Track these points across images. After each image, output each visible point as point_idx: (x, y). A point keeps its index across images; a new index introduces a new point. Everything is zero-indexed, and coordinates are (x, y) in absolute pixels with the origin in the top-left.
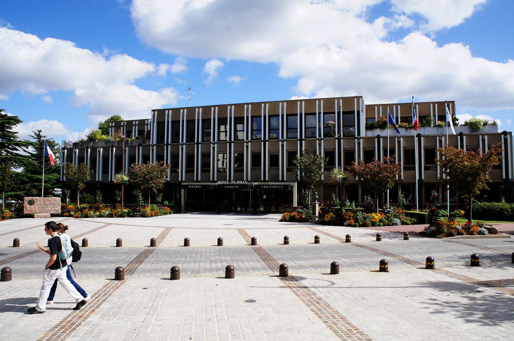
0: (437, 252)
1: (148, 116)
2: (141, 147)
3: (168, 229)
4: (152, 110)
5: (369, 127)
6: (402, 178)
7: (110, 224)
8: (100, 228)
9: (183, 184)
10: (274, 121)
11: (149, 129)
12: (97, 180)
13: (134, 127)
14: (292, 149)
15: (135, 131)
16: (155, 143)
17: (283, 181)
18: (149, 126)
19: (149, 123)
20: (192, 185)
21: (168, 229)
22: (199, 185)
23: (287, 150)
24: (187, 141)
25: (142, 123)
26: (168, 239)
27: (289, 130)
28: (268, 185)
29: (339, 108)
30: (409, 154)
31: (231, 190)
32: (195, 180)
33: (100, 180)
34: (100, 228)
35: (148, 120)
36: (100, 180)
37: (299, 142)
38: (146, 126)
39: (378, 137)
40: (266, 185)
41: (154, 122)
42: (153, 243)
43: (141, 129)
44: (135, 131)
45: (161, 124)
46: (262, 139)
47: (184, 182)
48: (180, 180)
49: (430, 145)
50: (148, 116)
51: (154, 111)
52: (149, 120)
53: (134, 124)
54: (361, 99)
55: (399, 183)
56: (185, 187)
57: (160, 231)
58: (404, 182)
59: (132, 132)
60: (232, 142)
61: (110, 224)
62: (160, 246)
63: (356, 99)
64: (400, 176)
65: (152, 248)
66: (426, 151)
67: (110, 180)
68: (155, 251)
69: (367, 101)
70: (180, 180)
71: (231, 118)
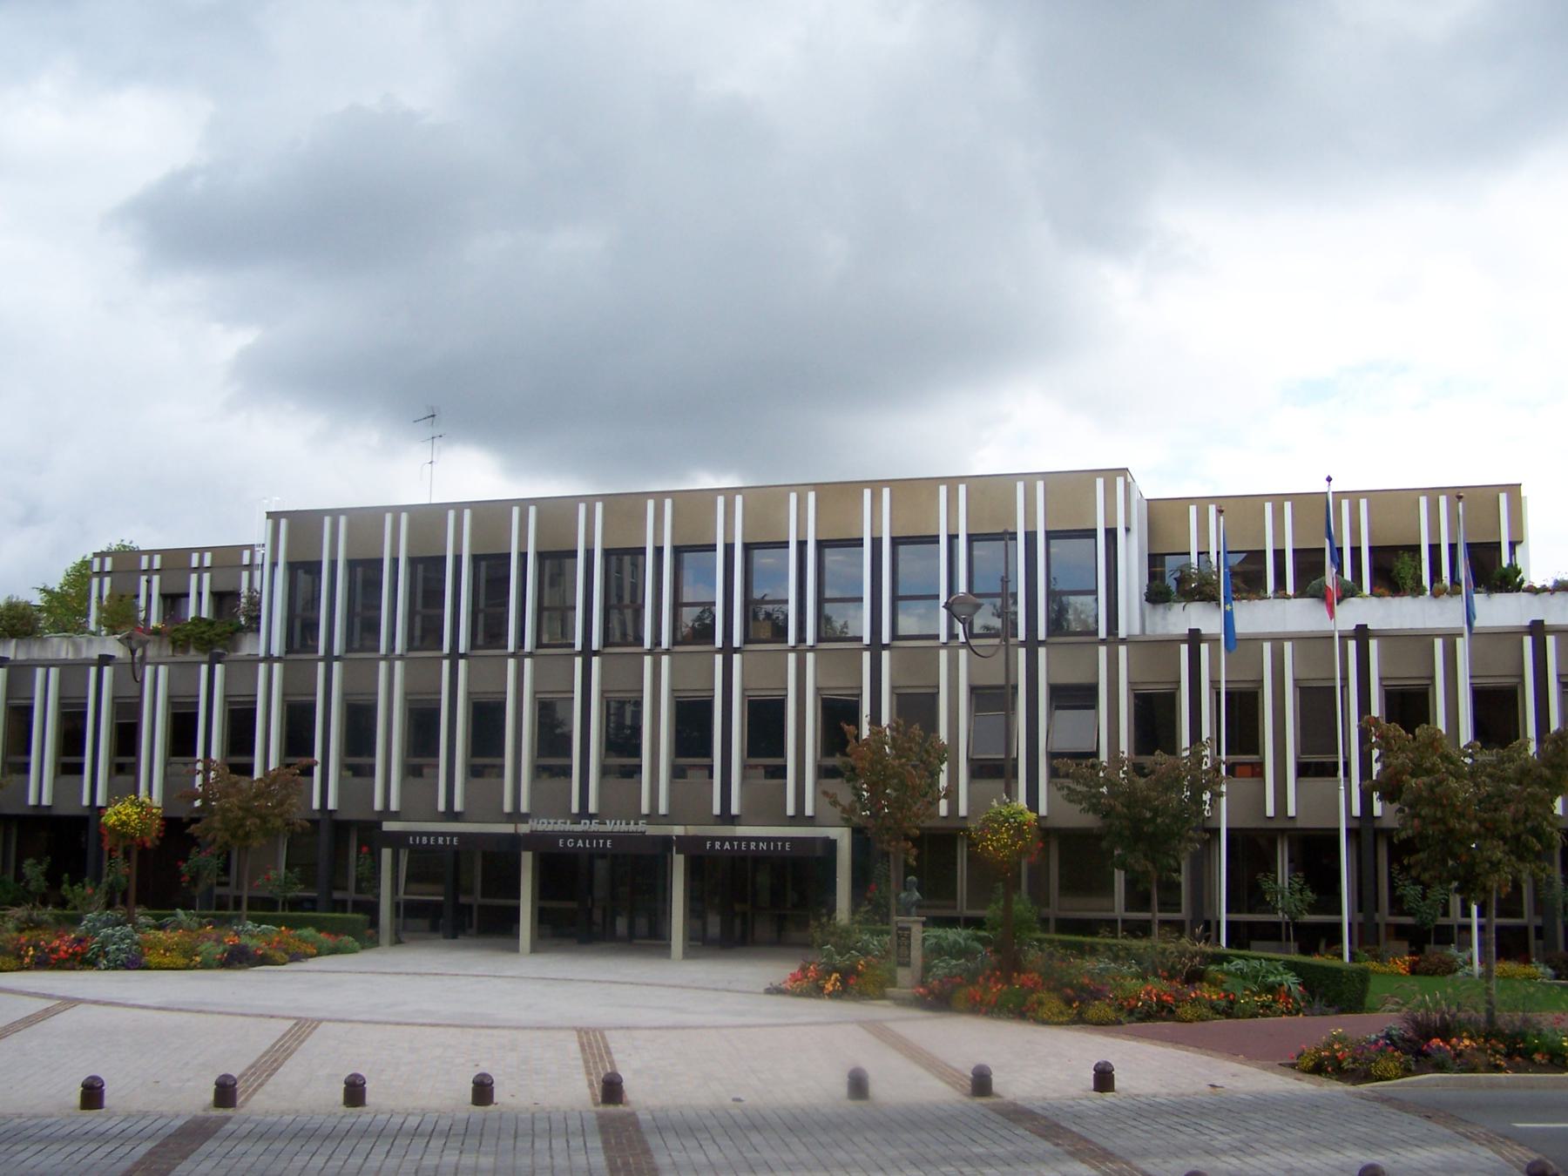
0: (1404, 1143)
1: (255, 532)
2: (219, 668)
3: (303, 1027)
4: (270, 515)
5: (1157, 595)
6: (1291, 812)
7: (71, 1002)
8: (29, 1021)
9: (388, 826)
10: (762, 558)
11: (257, 586)
12: (32, 801)
13: (194, 577)
14: (839, 686)
15: (200, 594)
16: (276, 650)
17: (799, 819)
18: (257, 574)
19: (258, 560)
20: (421, 834)
21: (303, 1027)
22: (452, 835)
23: (893, 688)
24: (410, 646)
25: (228, 559)
26: (291, 1073)
27: (901, 604)
28: (731, 839)
29: (1031, 516)
30: (1242, 709)
31: (593, 855)
32: (790, 811)
33: (331, 805)
34: (29, 1021)
35: (251, 547)
36: (46, 801)
37: (866, 656)
38: (245, 575)
39: (1362, 634)
40: (723, 839)
41: (274, 565)
42: (225, 1093)
43: (222, 587)
44: (200, 594)
45: (303, 571)
46: (1102, 634)
47: (395, 816)
48: (378, 805)
49: (1407, 674)
50: (255, 532)
51: (274, 516)
52: (259, 552)
53: (195, 563)
54: (1120, 481)
55: (1283, 831)
56: (396, 840)
57: (265, 1036)
58: (1299, 824)
59: (187, 595)
60: (596, 653)
61: (71, 1002)
62: (258, 1104)
63: (1100, 482)
64: (953, 806)
65: (221, 1112)
66: (1478, 695)
67: (316, 805)
68: (230, 1127)
69: (1151, 487)
70: (378, 805)
71: (523, 556)
